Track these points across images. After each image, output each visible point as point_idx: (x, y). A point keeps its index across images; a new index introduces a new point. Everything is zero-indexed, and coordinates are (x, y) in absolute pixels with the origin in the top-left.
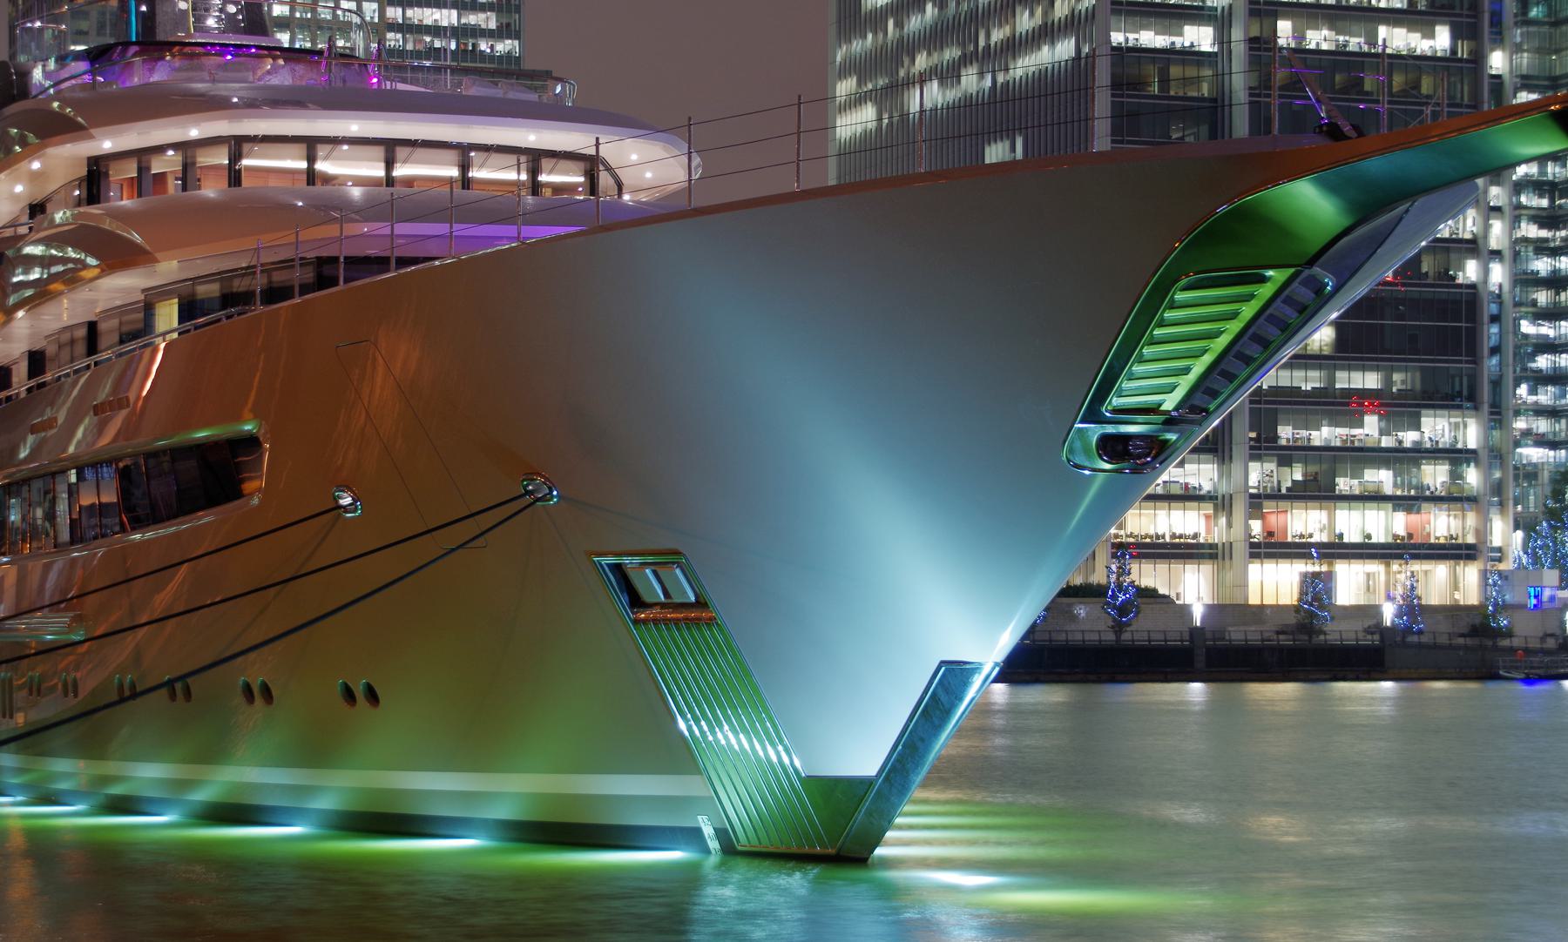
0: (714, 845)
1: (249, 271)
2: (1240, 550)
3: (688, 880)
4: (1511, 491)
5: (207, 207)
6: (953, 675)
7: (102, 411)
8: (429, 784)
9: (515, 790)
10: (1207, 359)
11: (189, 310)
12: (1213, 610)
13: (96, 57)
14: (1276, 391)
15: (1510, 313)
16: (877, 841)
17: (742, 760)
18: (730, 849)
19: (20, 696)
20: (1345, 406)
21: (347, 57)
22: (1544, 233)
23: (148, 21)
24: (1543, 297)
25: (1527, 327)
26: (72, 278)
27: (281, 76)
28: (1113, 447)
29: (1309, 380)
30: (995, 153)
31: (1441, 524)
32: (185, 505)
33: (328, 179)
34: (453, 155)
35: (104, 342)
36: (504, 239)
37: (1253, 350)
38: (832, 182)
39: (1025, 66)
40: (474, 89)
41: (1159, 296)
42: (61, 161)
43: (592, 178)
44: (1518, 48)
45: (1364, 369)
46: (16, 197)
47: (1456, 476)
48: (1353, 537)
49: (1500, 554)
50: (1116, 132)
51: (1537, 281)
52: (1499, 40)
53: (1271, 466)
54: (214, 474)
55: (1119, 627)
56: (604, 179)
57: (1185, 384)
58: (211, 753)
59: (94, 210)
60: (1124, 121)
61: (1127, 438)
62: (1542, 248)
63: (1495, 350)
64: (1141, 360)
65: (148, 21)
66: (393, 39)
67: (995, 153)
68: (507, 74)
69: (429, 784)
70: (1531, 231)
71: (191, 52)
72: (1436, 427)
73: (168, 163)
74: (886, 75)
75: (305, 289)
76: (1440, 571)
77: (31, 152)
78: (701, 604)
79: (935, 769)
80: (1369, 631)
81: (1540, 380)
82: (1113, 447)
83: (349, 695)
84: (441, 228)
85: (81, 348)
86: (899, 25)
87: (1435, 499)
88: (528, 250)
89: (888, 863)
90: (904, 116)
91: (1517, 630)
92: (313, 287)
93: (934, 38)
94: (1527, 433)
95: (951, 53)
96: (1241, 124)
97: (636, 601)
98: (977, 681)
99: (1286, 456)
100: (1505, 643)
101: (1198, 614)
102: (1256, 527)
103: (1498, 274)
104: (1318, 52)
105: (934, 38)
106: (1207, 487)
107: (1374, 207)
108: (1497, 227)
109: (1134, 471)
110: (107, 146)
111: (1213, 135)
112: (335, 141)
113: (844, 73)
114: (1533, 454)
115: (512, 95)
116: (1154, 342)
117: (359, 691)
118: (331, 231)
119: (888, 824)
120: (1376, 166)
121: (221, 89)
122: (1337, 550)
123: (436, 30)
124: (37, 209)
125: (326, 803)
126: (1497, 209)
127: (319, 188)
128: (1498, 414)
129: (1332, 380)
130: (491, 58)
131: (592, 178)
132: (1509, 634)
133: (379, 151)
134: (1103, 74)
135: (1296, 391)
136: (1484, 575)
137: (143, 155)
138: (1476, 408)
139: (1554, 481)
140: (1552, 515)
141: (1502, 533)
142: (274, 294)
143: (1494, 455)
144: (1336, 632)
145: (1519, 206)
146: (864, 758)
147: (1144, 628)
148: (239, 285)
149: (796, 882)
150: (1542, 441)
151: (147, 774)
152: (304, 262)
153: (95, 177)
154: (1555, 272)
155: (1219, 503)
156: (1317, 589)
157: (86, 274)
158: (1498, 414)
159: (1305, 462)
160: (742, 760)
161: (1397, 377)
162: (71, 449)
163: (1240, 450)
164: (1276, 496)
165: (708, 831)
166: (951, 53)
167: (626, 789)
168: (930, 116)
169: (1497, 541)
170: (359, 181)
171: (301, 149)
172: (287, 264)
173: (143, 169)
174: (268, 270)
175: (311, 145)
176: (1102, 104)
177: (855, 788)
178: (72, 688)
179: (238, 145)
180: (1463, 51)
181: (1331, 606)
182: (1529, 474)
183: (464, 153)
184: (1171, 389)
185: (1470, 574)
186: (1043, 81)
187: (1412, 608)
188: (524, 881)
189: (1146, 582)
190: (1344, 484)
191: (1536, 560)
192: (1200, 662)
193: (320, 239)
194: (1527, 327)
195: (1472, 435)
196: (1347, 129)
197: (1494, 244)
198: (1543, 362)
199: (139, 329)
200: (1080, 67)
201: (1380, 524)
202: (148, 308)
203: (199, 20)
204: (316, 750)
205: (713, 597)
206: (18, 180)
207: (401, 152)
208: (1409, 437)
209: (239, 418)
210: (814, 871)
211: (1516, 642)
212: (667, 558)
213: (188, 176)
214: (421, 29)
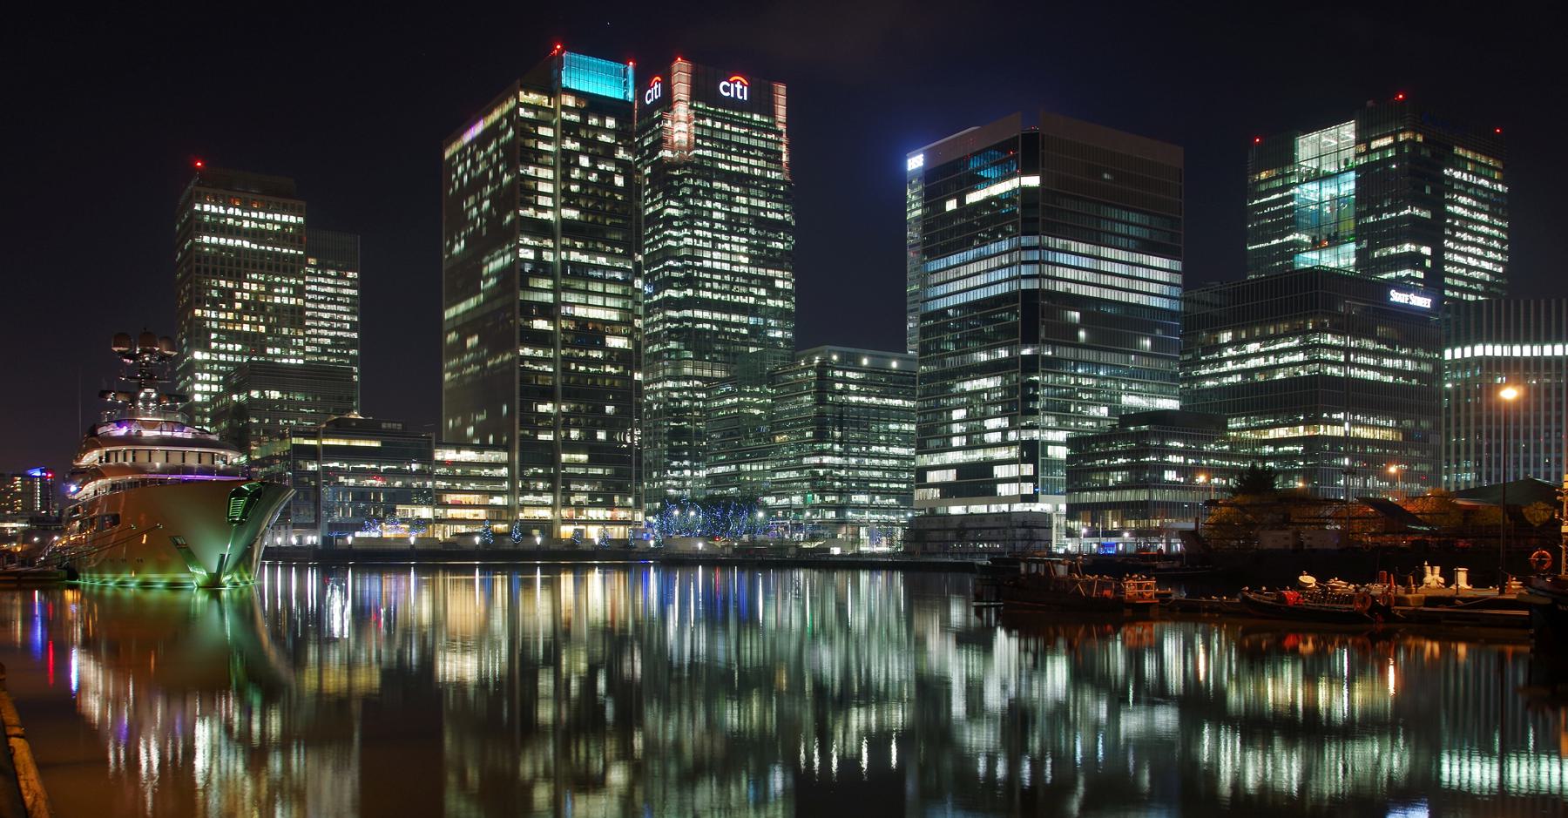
29: (581, 471)
52: (639, 370)
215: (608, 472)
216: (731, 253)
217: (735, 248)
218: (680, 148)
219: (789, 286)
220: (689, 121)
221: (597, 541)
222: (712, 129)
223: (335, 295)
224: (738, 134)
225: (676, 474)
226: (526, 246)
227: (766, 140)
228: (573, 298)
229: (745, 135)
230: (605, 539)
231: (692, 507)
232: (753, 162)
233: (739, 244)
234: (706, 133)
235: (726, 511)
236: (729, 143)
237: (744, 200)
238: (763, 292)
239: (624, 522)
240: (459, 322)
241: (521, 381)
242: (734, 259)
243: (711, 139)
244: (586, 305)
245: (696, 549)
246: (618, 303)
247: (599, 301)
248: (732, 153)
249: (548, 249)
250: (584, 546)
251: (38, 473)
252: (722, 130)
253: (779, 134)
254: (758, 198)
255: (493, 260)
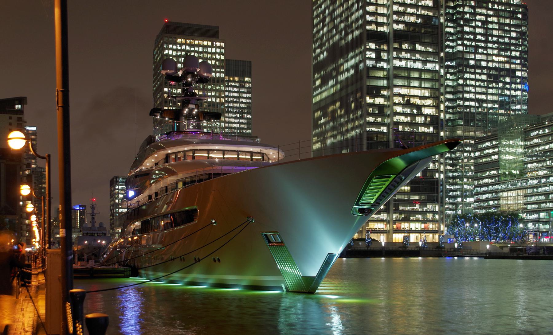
0: (285, 290)
1: (195, 176)
2: (392, 231)
3: (279, 298)
4: (445, 219)
5: (188, 163)
6: (331, 256)
7: (168, 204)
8: (230, 278)
9: (247, 279)
10: (379, 193)
11: (184, 184)
12: (387, 243)
13: (168, 134)
14: (399, 199)
15: (445, 184)
16: (316, 289)
17: (291, 273)
18: (288, 291)
19: (153, 260)
20: (412, 203)
21: (217, 133)
22: (451, 168)
23: (178, 127)
24: (451, 181)
25: (448, 187)
26: (162, 178)
27: (204, 137)
28: (361, 211)
29: (405, 198)
30: (344, 152)
31: (431, 226)
32: (183, 223)
33: (212, 158)
34: (236, 153)
35: (169, 190)
36: (244, 169)
37: (388, 191)
38: (312, 157)
39: (349, 135)
40: (240, 140)
41: (370, 181)
42: (162, 154)
43: (263, 157)
44: (446, 131)
45: (416, 195)
46: (153, 162)
47: (434, 216)
48: (413, 229)
49: (442, 232)
50: (367, 147)
51: (450, 178)
52: (442, 130)
53: (398, 215)
54: (189, 216)
55: (368, 247)
56: (265, 157)
57: (375, 198)
58: (189, 272)
59: (166, 164)
60: (370, 146)
61: (364, 209)
62: (451, 171)
63: (441, 191)
64: (366, 193)
65: (178, 127)
66: (227, 130)
67: (344, 152)
68: (249, 137)
69: (230, 278)
70: (449, 168)
71: (186, 133)
72: (430, 207)
73: (181, 155)
74: (323, 137)
75: (206, 180)
76: (431, 235)
77: (155, 153)
78: (282, 242)
79: (327, 274)
80: (416, 247)
81: (450, 197)
82: (361, 211)
83: (215, 260)
84: (231, 167)
85: (164, 192)
86: (325, 127)
87: (430, 221)
88: (248, 172)
89: (318, 293)
90: (326, 145)
91: (446, 247)
92: (207, 178)
93: (332, 129)
94: (448, 208)
95: (335, 132)
96: (392, 145)
97: (269, 242)
98: (335, 257)
99: (401, 212)
100: (443, 250)
101: (383, 244)
102: (395, 226)
103: (442, 176)
104: (407, 132)
105: (332, 129)
106: (385, 219)
107: (412, 164)
108: (442, 167)
109: (366, 215)
110: (169, 152)
111: (387, 148)
112: (213, 150)
113: (314, 136)
114: (449, 212)
115: (248, 141)
116: (369, 190)
117: (216, 260)
118: (210, 168)
119: (318, 286)
120: (412, 154)
121: (191, 140)
122: (410, 231)
123: (235, 128)
124: (156, 164)
125: (211, 281)
126: (442, 163)
127: (210, 160)
128: (442, 204)
129: (410, 197)
130: (246, 134)
131: (263, 157)
132: (444, 248)
133: (207, 152)
134: (365, 136)
135: (402, 199)
136: (439, 236)
137: (176, 153)
138: (438, 203)
139: (453, 217)
140: (453, 224)
141: (442, 228)
142: (200, 181)
143: (441, 212)
144: (410, 248)
145: (446, 163)
146: (313, 273)
147: (373, 247)
148: (194, 179)
149: (301, 297)
150: (450, 209)
151: (177, 276)
152: (206, 174)
153: (167, 157)
154: (453, 176)
155: (387, 222)
156: (407, 239)
157: (165, 177)
158: (442, 204)
159: (404, 214)
160: (291, 273)
161: (422, 197)
162: (163, 211)
163: (392, 211)
164: (399, 220)
165: (284, 287)
166: (335, 132)
167: (268, 279)
168: (331, 145)
169: (442, 229)
170: (218, 158)
171: (222, 152)
172: (202, 175)
173: (176, 156)
174: (198, 176)
175: (208, 151)
176: (365, 142)
177: (312, 278)
178: (162, 259)
179: (194, 151)
180: (435, 132)
181: (409, 242)
182: (448, 216)
183: (238, 153)
184: (372, 199)
185: (436, 236)
186: (353, 138)
187: (425, 243)
188: (248, 297)
189: (373, 238)
190: (412, 218)
191: (449, 233)
192: (384, 254)
193: (208, 170)
194: (448, 187)
195: (437, 208)
196: (406, 147)
197: (441, 170)
198: (451, 194)
199: (175, 186)
200: (360, 136)
201: (419, 226)
202: (177, 184)
203: (188, 126)
204: (208, 271)
205: (284, 241)
206: (153, 159)
207: (226, 152)
208: (425, 209)
209: (193, 205)
210: (304, 296)
211: (445, 250)
212: (275, 233)
213: (185, 157)
214: (232, 128)
215: (423, 197)
216: (488, 54)
219: (525, 75)
223: (239, 98)
226: (370, 50)
228: (400, 82)
230: (425, 243)
233: (492, 48)
237: (495, 20)
238: (508, 80)
239: (433, 232)
240: (323, 104)
244: (409, 87)
245: (86, 245)
246: (428, 85)
247: (415, 84)
249: (384, 51)
254: (505, 17)
255: (347, 61)
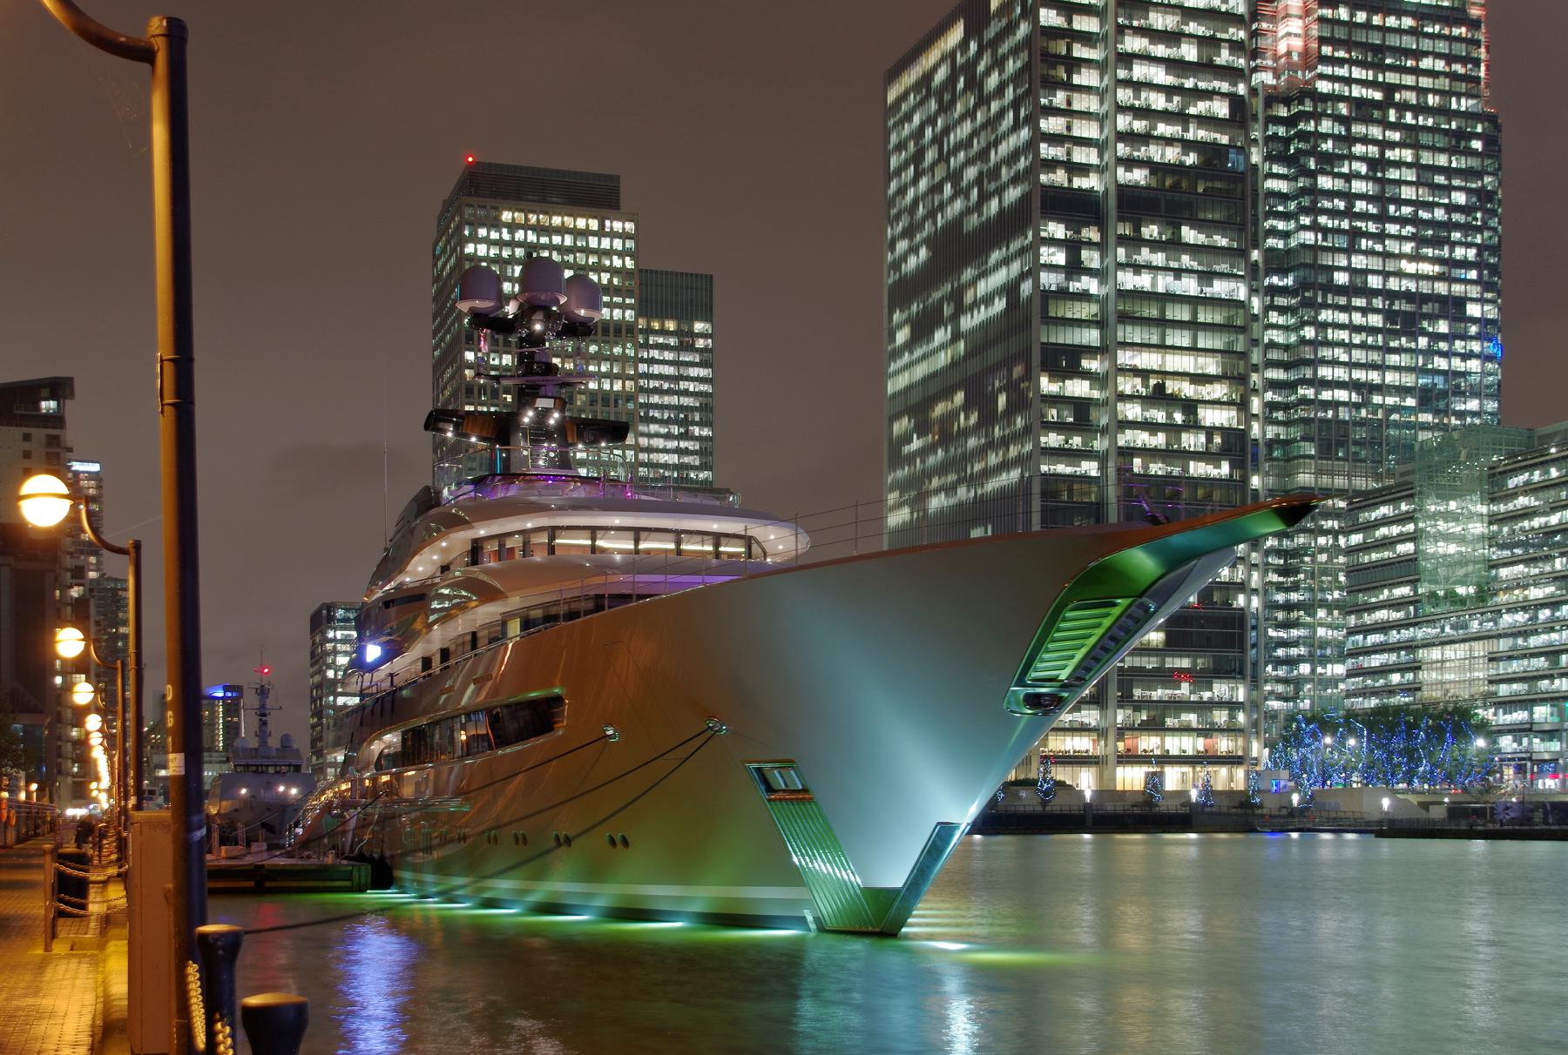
217: (1392, 246)
218: (1291, 67)
219: (1491, 312)
220: (1307, 12)
221: (1088, 796)
222: (1350, 25)
224: (1399, 31)
225: (1282, 672)
226: (1052, 242)
227: (1450, 39)
228: (1135, 334)
229: (1412, 32)
230: (1208, 791)
231: (1351, 731)
232: (1425, 82)
234: (1340, 33)
235: (1410, 736)
236: (1380, 50)
237: (1408, 155)
239: (1231, 760)
240: (915, 398)
241: (1044, 494)
242: (1391, 266)
243: (1348, 44)
244: (1162, 347)
246: (1217, 342)
247: (1180, 338)
248: (1384, 68)
249: (1090, 244)
250: (1165, 806)
251: (220, 694)
252: (1368, 26)
253: (1474, 24)
254: (1433, 149)
255: (984, 274)
